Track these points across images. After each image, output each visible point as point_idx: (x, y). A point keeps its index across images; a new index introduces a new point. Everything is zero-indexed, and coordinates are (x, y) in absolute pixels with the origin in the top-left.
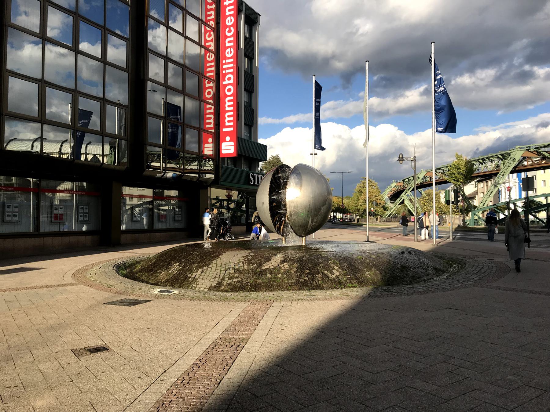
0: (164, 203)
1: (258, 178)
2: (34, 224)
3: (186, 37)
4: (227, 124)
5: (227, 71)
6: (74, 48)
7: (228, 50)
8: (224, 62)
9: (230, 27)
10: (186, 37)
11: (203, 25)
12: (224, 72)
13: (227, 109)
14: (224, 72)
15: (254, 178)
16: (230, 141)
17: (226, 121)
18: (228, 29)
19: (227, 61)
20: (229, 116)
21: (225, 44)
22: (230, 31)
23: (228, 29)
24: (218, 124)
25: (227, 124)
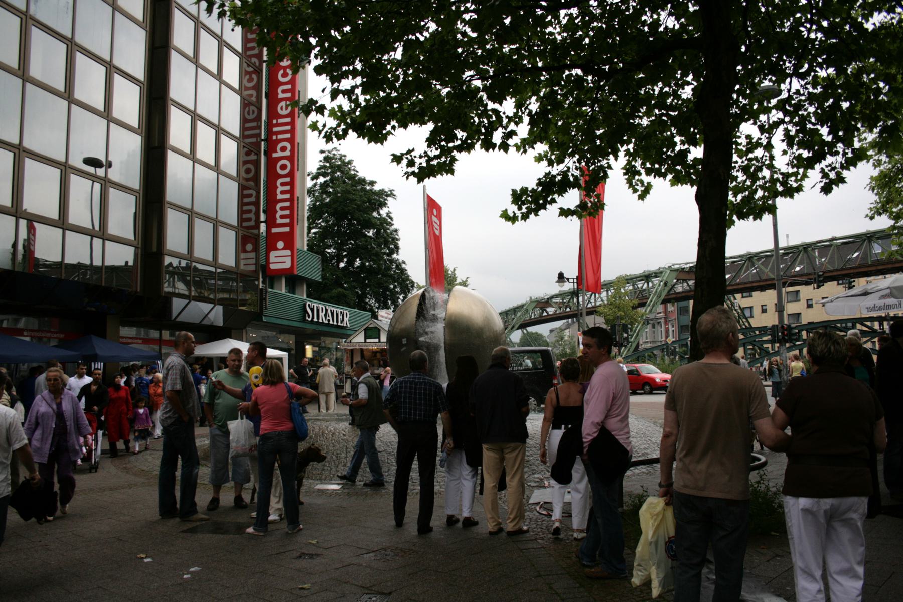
0: (877, 249)
1: (318, 310)
2: (408, 508)
3: (222, 82)
4: (279, 221)
5: (280, 137)
6: (13, 210)
7: (283, 104)
8: (275, 122)
9: (285, 68)
10: (222, 82)
11: (97, 228)
12: (274, 138)
13: (280, 196)
14: (274, 138)
15: (312, 310)
16: (284, 249)
17: (278, 216)
18: (282, 72)
19: (281, 121)
20: (282, 208)
21: (278, 94)
22: (285, 75)
23: (282, 72)
24: (52, 332)
25: (279, 221)
